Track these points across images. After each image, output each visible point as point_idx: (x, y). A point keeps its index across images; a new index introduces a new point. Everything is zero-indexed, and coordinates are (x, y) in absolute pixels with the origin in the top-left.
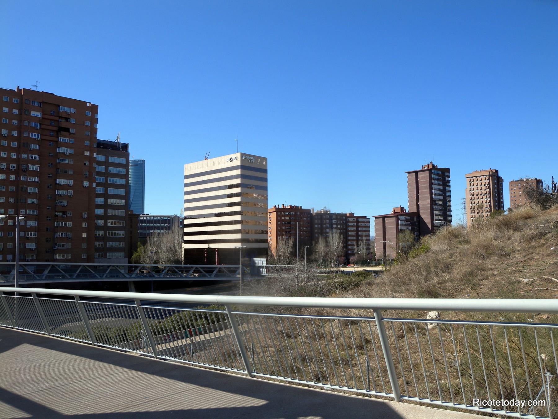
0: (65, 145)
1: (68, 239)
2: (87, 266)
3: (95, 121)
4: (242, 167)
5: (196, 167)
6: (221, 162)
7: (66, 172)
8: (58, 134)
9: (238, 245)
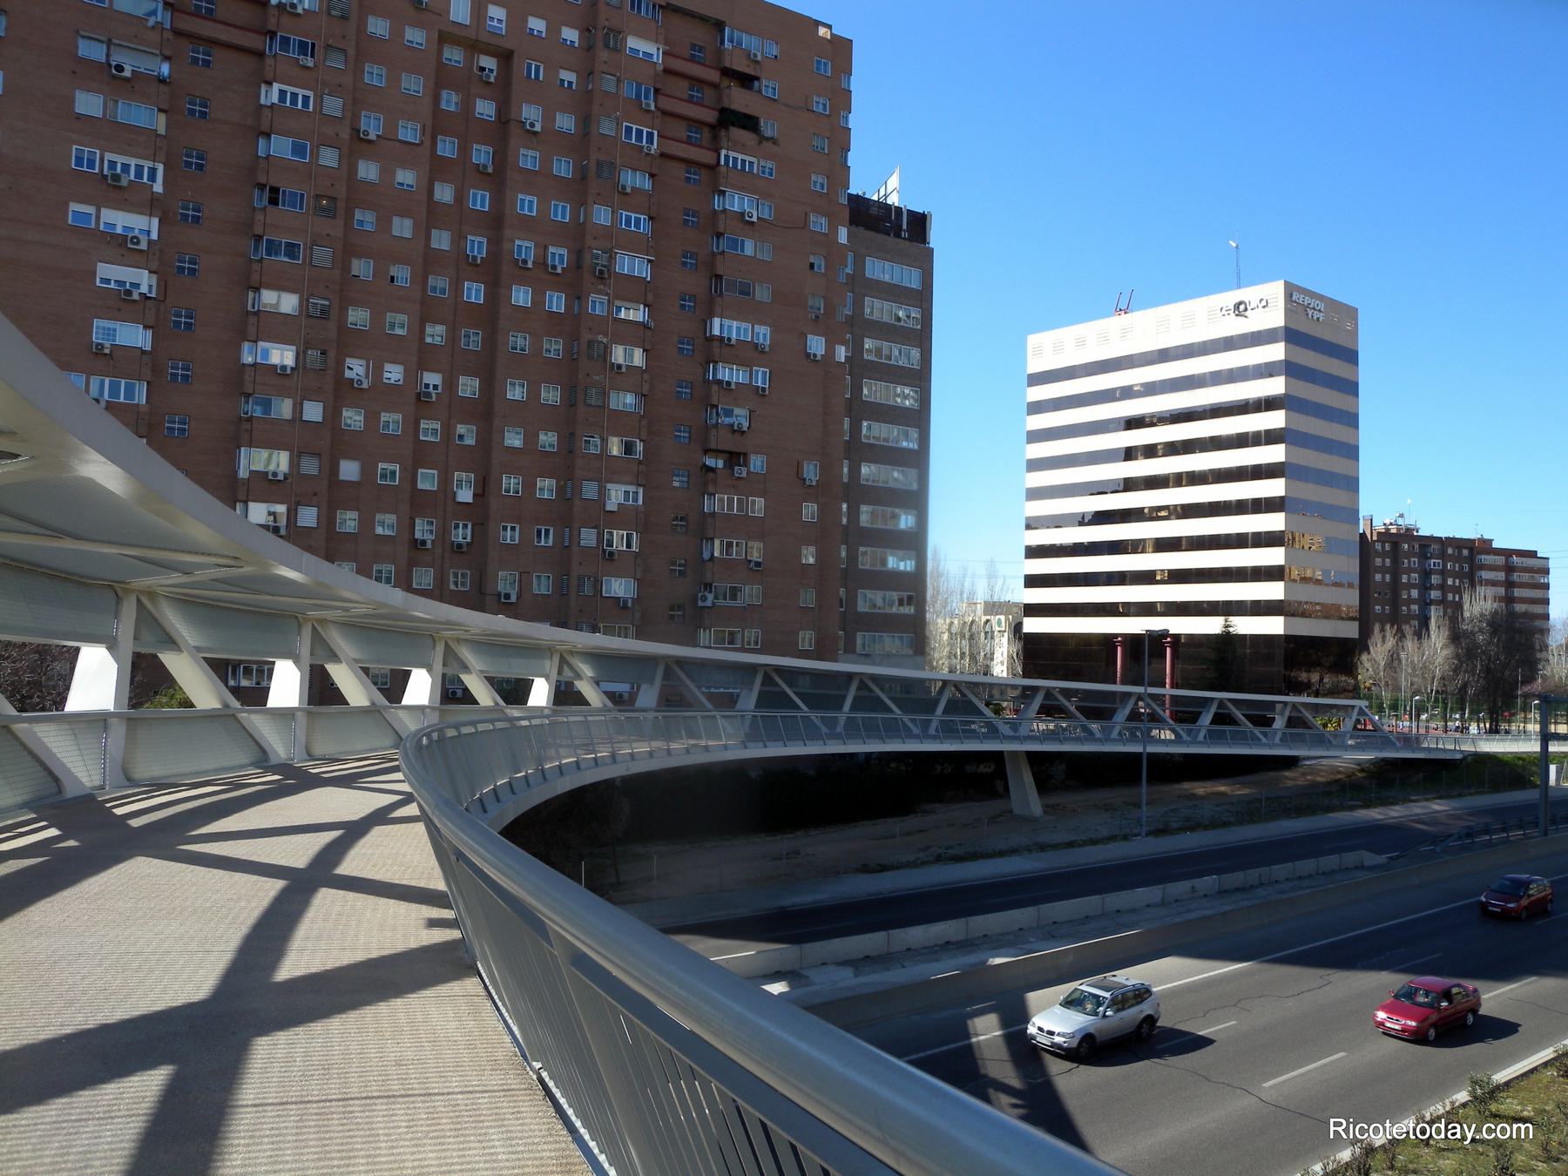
0: (747, 182)
1: (755, 569)
2: (1231, 701)
3: (842, 100)
4: (1290, 335)
5: (1081, 343)
6: (1200, 317)
7: (746, 291)
8: (715, 138)
9: (1273, 626)
